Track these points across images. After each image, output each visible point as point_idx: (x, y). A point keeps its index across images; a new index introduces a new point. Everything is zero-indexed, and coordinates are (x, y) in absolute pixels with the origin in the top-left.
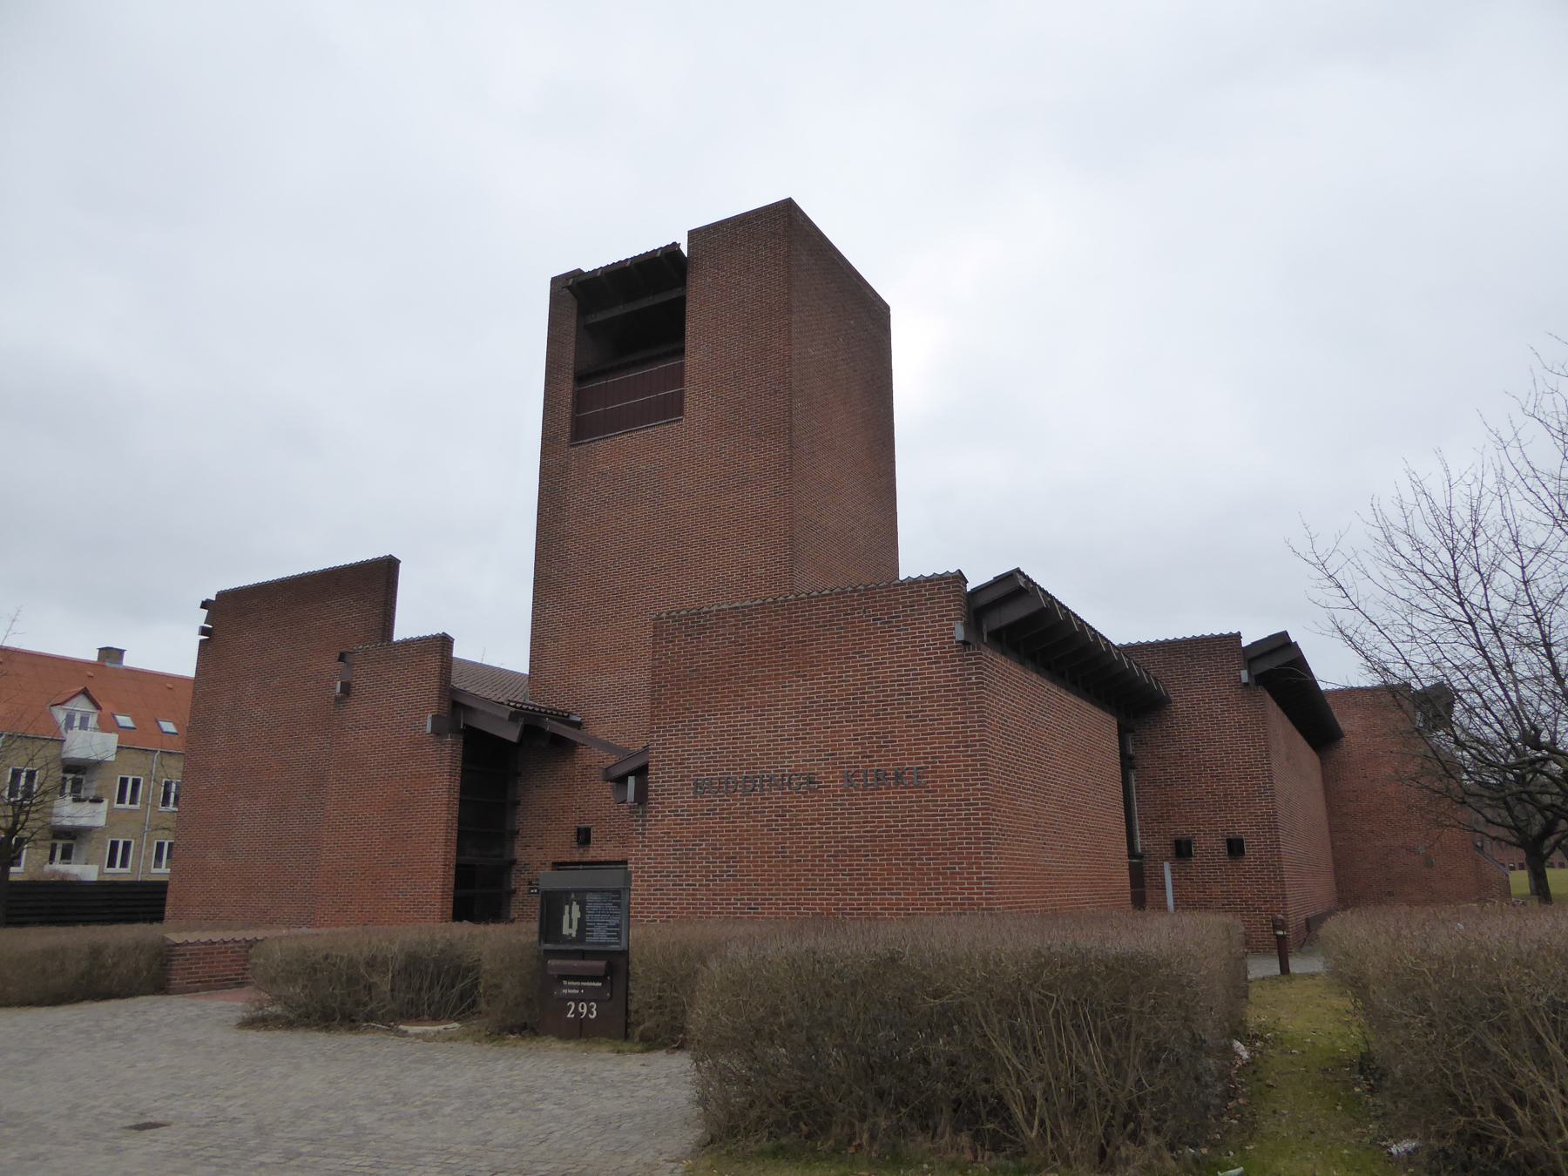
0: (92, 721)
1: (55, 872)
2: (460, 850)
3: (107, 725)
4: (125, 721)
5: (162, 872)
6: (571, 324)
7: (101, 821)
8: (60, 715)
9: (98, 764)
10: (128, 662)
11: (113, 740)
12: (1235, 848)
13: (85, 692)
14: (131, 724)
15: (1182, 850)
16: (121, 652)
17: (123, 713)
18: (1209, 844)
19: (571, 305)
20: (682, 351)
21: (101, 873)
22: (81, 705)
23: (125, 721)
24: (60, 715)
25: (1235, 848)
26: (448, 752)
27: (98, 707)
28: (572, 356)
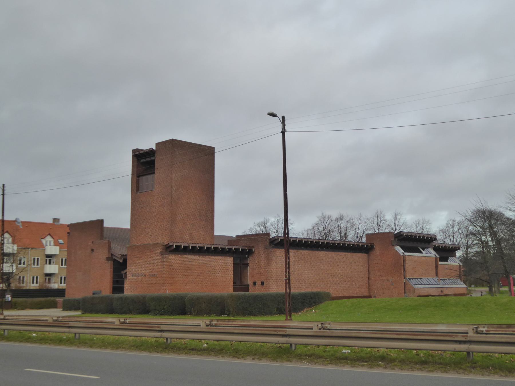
0: (52, 242)
1: (46, 286)
2: (113, 284)
3: (56, 244)
4: (61, 241)
5: (63, 286)
6: (136, 163)
7: (57, 271)
8: (44, 241)
9: (55, 255)
10: (61, 222)
11: (58, 248)
12: (263, 283)
13: (49, 234)
14: (63, 243)
15: (255, 284)
16: (59, 219)
17: (60, 239)
18: (259, 283)
19: (136, 159)
20: (154, 173)
21: (59, 286)
22: (49, 238)
23: (61, 241)
24: (44, 241)
25: (263, 283)
26: (110, 263)
27: (53, 238)
28: (29, 299)
